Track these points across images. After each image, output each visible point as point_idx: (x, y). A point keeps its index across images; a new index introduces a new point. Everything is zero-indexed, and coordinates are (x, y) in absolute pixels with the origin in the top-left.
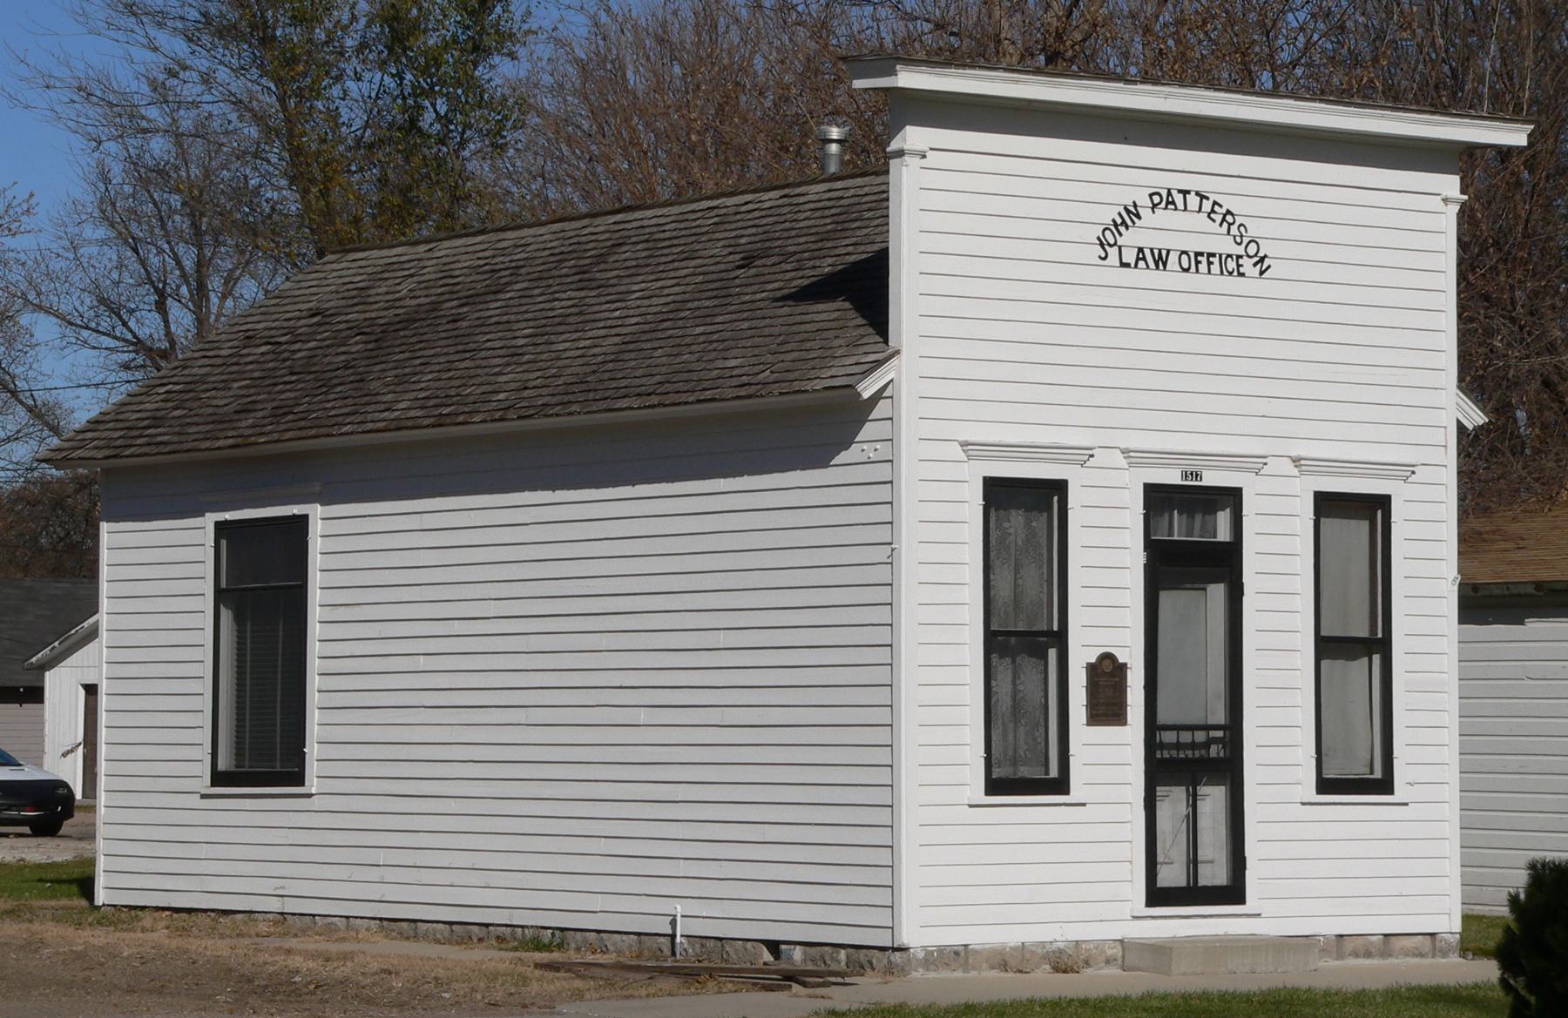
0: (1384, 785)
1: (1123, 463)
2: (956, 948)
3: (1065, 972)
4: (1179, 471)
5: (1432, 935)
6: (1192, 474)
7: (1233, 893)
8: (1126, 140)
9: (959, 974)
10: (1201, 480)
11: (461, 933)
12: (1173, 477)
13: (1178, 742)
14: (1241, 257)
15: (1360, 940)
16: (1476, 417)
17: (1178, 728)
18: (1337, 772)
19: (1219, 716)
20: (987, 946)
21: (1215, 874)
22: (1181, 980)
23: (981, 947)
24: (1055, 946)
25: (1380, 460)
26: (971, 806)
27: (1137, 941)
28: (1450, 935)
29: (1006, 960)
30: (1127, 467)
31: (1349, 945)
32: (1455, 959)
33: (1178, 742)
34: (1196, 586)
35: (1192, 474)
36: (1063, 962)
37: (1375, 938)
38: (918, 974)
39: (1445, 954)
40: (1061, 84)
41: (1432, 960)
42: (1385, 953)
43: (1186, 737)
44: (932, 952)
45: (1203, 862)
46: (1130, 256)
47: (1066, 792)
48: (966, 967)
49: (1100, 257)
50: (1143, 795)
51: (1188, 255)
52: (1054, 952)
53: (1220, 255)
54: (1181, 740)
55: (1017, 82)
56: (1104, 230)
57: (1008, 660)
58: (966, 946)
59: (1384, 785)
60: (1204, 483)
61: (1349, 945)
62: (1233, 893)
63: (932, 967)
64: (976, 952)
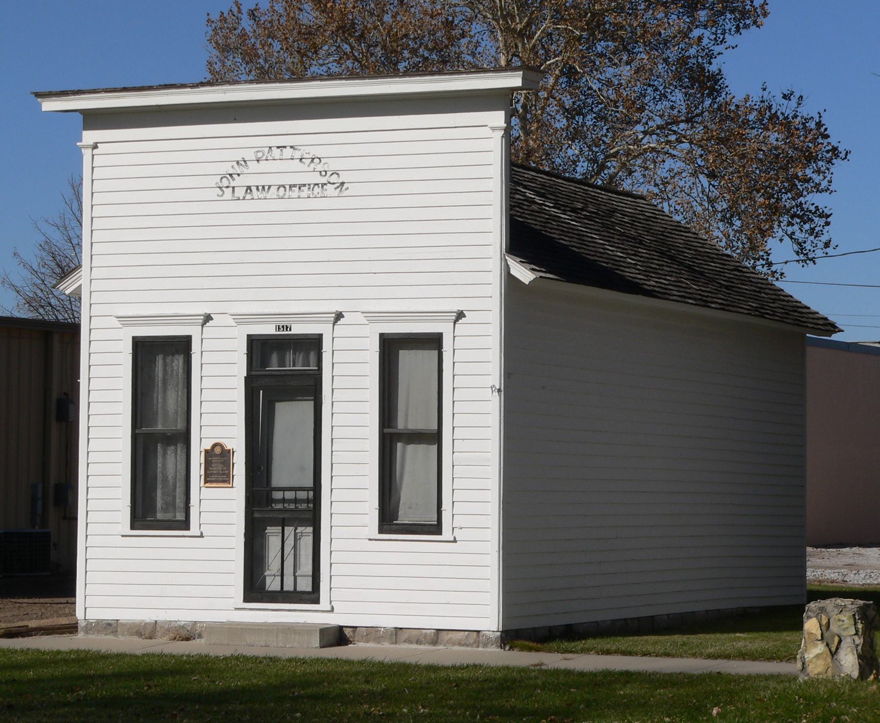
0: (436, 529)
1: (118, 325)
2: (110, 621)
3: (188, 639)
4: (274, 326)
5: (478, 632)
6: (283, 327)
7: (313, 596)
8: (235, 120)
9: (111, 637)
10: (290, 330)
11: (592, 622)
12: (268, 329)
13: (284, 498)
14: (325, 184)
15: (415, 632)
16: (530, 277)
17: (284, 489)
18: (418, 519)
19: (310, 483)
20: (130, 622)
21: (305, 585)
22: (255, 648)
23: (127, 621)
24: (179, 623)
25: (425, 310)
26: (123, 536)
27: (287, 624)
28: (491, 633)
29: (149, 630)
30: (121, 326)
31: (404, 635)
32: (494, 649)
33: (284, 498)
34: (305, 398)
35: (283, 327)
36: (186, 633)
37: (428, 631)
38: (81, 635)
39: (485, 645)
40: (146, 95)
41: (476, 649)
42: (435, 642)
43: (289, 495)
44: (93, 622)
45: (308, 576)
46: (240, 192)
47: (188, 528)
48: (115, 632)
49: (218, 195)
50: (243, 531)
51: (285, 187)
52: (175, 627)
53: (309, 185)
54: (297, 498)
55: (119, 97)
56: (222, 178)
57: (173, 447)
58: (117, 620)
59: (436, 529)
60: (293, 332)
61: (404, 635)
62: (313, 596)
63: (91, 632)
64: (123, 625)
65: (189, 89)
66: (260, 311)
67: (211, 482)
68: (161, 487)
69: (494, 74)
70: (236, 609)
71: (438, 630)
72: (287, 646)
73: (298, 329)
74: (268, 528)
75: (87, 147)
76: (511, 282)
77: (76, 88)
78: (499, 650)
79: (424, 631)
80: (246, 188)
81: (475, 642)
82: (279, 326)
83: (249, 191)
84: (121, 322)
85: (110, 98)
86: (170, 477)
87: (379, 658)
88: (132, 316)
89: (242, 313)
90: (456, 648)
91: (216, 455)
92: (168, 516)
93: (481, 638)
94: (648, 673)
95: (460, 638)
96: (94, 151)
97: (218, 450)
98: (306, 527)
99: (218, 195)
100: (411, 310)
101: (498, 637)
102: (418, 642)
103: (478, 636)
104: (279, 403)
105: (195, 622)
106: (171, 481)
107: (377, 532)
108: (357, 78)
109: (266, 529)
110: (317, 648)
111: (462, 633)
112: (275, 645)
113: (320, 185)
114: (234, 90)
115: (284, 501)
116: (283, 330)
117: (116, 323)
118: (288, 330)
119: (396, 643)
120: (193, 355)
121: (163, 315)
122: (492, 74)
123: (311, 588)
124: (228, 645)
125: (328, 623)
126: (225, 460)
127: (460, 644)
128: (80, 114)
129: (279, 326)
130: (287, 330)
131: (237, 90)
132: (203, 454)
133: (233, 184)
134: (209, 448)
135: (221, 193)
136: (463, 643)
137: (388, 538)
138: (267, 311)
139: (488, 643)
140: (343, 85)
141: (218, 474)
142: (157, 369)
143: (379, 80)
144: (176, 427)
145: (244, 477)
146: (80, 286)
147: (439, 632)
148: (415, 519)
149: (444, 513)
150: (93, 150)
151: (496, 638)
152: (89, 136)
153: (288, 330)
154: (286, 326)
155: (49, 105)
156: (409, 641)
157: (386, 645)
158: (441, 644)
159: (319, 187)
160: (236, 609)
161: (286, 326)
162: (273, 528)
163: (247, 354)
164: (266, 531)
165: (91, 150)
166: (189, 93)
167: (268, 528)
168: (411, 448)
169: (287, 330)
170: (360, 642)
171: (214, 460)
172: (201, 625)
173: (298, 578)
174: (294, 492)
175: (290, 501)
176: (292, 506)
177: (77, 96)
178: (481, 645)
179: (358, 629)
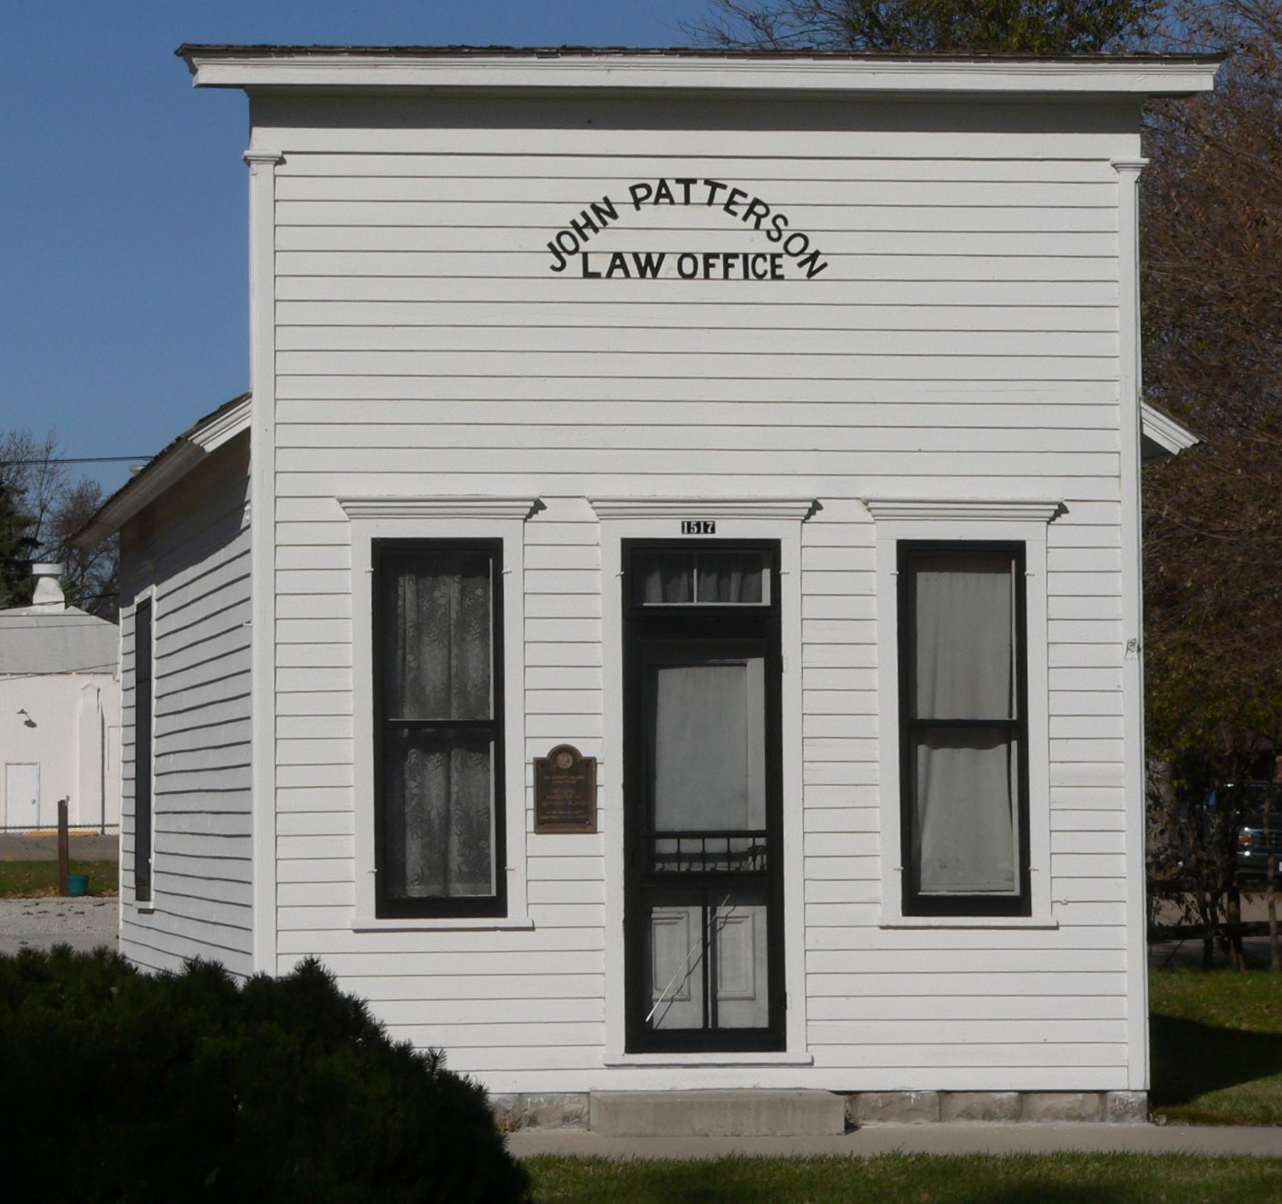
0: (1019, 905)
1: (592, 515)
5: (1102, 1093)
8: (590, 124)
10: (713, 531)
12: (670, 530)
19: (758, 822)
28: (1130, 1094)
32: (1137, 1124)
35: (698, 525)
37: (1005, 1095)
39: (1119, 1117)
41: (1102, 1125)
42: (1017, 1116)
47: (502, 913)
49: (553, 268)
50: (622, 916)
54: (733, 850)
55: (376, 66)
59: (1019, 905)
60: (719, 535)
61: (960, 1103)
65: (534, 59)
66: (645, 494)
67: (550, 822)
68: (457, 831)
69: (1164, 65)
70: (610, 1066)
71: (1023, 1093)
72: (779, 1133)
73: (727, 530)
74: (655, 909)
75: (262, 160)
76: (1150, 451)
77: (289, 43)
78: (1147, 1125)
79: (998, 1096)
80: (611, 255)
81: (1097, 1112)
82: (689, 524)
83: (618, 262)
84: (600, 511)
85: (357, 65)
86: (433, 814)
87: (912, 1147)
88: (675, 498)
89: (1045, 500)
90: (1062, 1124)
91: (560, 771)
92: (435, 890)
93: (1109, 1105)
94: (838, 1158)
95: (1069, 1106)
96: (278, 167)
97: (565, 762)
98: (735, 905)
99: (553, 268)
100: (960, 498)
101: (1143, 1102)
102: (988, 1115)
103: (1103, 1102)
104: (668, 671)
105: (520, 1094)
106: (437, 822)
107: (900, 913)
108: (877, 56)
109: (651, 912)
110: (838, 1134)
111: (1072, 1097)
112: (754, 1131)
113: (768, 257)
114: (630, 65)
115: (679, 857)
116: (699, 532)
117: (337, 511)
118: (709, 530)
119: (940, 1119)
120: (505, 576)
121: (606, 498)
122: (1159, 65)
123: (766, 1017)
124: (654, 1135)
125: (803, 1086)
126: (579, 781)
127: (1069, 1117)
128: (246, 95)
129: (689, 524)
130: (706, 531)
131: (638, 65)
132: (531, 769)
133: (584, 246)
134: (544, 754)
135: (558, 264)
136: (1074, 1114)
137: (925, 924)
138: (661, 494)
139: (1126, 1112)
140: (859, 68)
141: (565, 808)
142: (400, 603)
143: (474, 59)
144: (449, 716)
145: (621, 813)
146: (247, 432)
147: (1025, 1096)
148: (959, 888)
149: (509, 875)
150: (275, 165)
151: (1140, 1104)
152: (267, 140)
153: (709, 530)
154: (705, 523)
155: (210, 72)
156: (969, 1115)
157: (926, 1125)
158: (1029, 1117)
159: (765, 260)
160: (610, 1066)
161: (705, 523)
162: (665, 909)
163: (622, 576)
164: (653, 916)
165: (272, 166)
166: (973, 71)
167: (655, 909)
168: (941, 755)
169: (706, 531)
170: (870, 1119)
171: (557, 780)
172: (536, 1100)
173: (720, 1004)
174: (701, 841)
175: (691, 858)
176: (697, 867)
177: (287, 59)
178: (1109, 1116)
179: (1109, 1094)
